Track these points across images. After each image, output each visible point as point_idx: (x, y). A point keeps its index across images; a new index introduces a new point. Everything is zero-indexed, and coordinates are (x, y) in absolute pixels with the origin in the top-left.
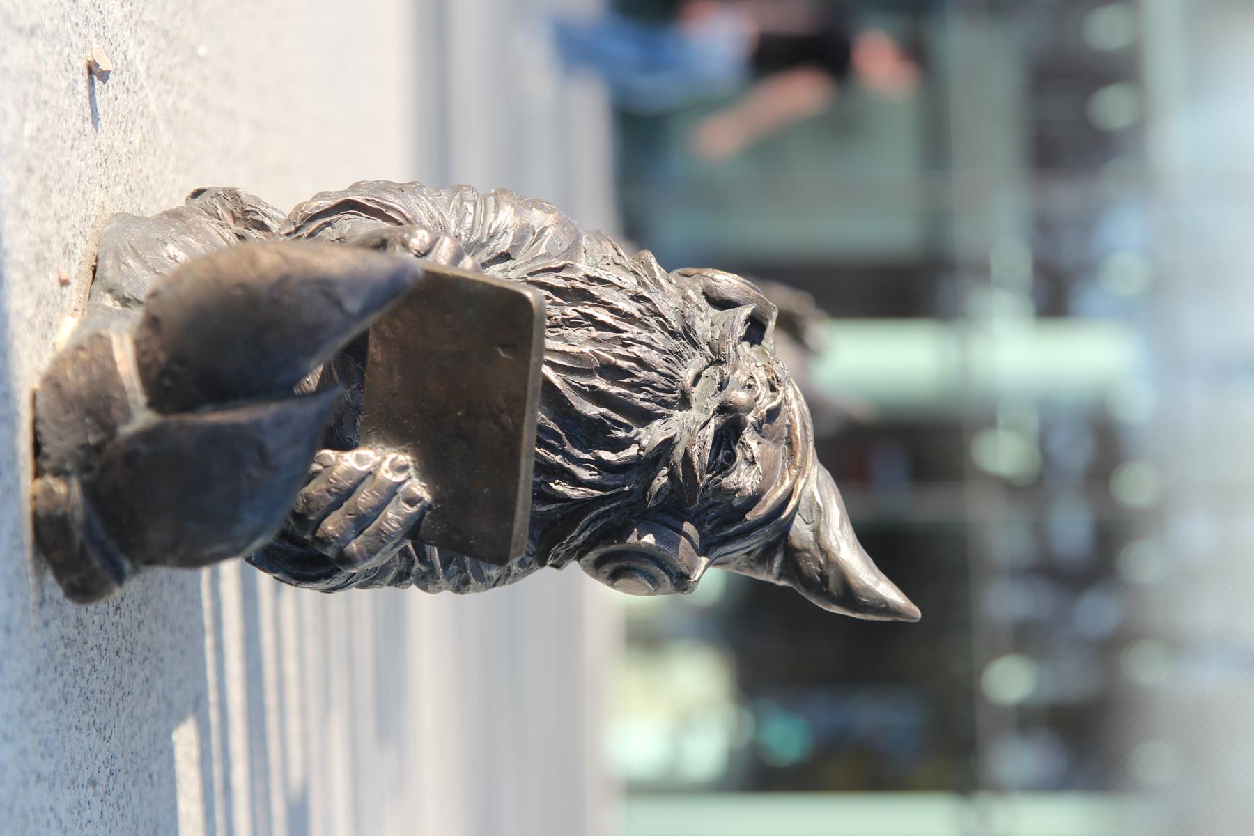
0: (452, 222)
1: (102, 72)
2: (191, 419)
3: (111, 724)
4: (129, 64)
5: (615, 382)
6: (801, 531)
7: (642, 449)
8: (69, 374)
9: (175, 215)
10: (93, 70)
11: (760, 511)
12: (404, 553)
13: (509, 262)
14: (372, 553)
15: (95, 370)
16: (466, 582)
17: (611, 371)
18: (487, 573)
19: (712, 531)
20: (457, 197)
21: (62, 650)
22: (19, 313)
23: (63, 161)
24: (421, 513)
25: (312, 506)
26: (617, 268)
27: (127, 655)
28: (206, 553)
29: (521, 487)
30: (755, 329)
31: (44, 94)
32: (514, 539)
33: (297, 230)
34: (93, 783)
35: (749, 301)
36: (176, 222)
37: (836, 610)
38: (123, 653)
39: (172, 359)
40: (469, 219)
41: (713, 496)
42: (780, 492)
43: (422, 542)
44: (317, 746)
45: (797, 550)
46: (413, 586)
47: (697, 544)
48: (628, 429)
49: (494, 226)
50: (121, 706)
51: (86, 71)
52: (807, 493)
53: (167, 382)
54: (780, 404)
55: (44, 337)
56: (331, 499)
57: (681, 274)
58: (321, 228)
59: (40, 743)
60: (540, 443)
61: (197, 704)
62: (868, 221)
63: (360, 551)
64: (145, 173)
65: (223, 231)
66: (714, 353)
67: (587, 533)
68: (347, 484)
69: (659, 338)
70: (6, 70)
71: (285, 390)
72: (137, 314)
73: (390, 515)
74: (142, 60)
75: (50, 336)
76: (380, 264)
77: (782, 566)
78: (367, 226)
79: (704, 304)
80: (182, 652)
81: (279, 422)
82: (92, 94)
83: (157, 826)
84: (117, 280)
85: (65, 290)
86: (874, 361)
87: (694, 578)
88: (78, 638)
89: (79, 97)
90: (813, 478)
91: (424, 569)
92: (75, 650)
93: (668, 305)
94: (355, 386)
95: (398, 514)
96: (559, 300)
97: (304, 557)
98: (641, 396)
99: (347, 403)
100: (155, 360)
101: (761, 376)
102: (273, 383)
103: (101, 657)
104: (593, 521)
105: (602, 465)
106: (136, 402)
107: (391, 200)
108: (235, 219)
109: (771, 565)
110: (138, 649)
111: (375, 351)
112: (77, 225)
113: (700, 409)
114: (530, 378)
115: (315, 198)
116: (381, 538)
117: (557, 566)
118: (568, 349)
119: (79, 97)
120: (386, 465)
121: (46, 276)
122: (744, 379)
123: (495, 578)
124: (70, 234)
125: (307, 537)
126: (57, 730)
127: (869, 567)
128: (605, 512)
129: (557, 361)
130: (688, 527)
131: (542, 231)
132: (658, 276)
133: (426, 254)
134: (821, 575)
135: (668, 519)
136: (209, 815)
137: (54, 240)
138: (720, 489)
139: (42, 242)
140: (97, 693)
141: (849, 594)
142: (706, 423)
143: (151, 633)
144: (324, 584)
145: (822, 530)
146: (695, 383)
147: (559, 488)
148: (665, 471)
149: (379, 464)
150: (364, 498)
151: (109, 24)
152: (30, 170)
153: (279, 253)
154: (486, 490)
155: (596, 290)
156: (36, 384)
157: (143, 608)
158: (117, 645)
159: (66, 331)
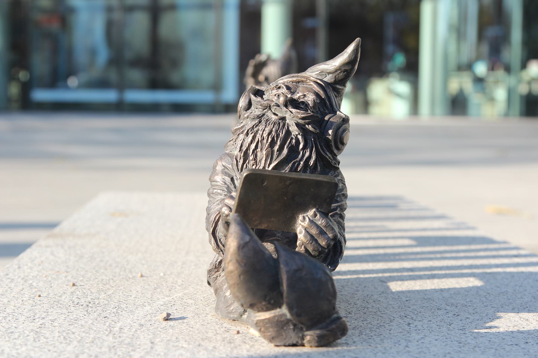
2: (285, 295)
4: (165, 304)
5: (276, 143)
6: (329, 79)
7: (299, 134)
8: (269, 334)
9: (216, 291)
10: (167, 318)
11: (322, 93)
12: (332, 216)
14: (333, 229)
15: (268, 325)
16: (344, 195)
17: (272, 144)
18: (341, 187)
21: (363, 336)
23: (197, 332)
24: (319, 212)
25: (316, 249)
26: (237, 141)
27: (366, 309)
28: (331, 290)
29: (311, 178)
30: (259, 93)
31: (174, 338)
32: (329, 181)
33: (222, 251)
34: (409, 324)
36: (219, 291)
37: (356, 67)
38: (365, 311)
39: (265, 300)
40: (219, 191)
42: (315, 86)
44: (397, 233)
45: (335, 80)
48: (292, 139)
51: (167, 321)
52: (315, 76)
53: (272, 302)
55: (256, 341)
56: (314, 243)
58: (221, 243)
61: (384, 281)
63: (332, 233)
64: (202, 298)
65: (222, 276)
67: (328, 153)
68: (309, 237)
69: (261, 127)
70: (165, 354)
71: (276, 262)
72: (248, 310)
73: (320, 223)
76: (234, 228)
78: (221, 227)
79: (250, 111)
80: (365, 287)
81: (287, 264)
83: (424, 298)
85: (240, 332)
87: (344, 116)
90: (311, 74)
91: (339, 209)
92: (363, 331)
93: (250, 124)
95: (319, 220)
96: (247, 161)
97: (334, 252)
99: (281, 235)
100: (265, 305)
101: (275, 92)
102: (272, 266)
104: (323, 151)
105: (304, 148)
106: (279, 312)
107: (212, 218)
108: (218, 271)
111: (263, 226)
112: (219, 326)
113: (286, 113)
114: (274, 174)
116: (327, 226)
117: (339, 163)
118: (264, 159)
120: (303, 224)
121: (236, 339)
122: (276, 98)
124: (222, 329)
125: (327, 251)
126: (391, 339)
130: (326, 118)
131: (224, 166)
133: (230, 208)
134: (344, 72)
136: (420, 277)
138: (313, 107)
141: (351, 63)
142: (291, 112)
144: (343, 244)
146: (277, 115)
148: (307, 126)
149: (302, 226)
150: (314, 231)
151: (151, 311)
152: (199, 345)
153: (228, 263)
155: (244, 149)
156: (272, 345)
157: (349, 303)
159: (254, 332)
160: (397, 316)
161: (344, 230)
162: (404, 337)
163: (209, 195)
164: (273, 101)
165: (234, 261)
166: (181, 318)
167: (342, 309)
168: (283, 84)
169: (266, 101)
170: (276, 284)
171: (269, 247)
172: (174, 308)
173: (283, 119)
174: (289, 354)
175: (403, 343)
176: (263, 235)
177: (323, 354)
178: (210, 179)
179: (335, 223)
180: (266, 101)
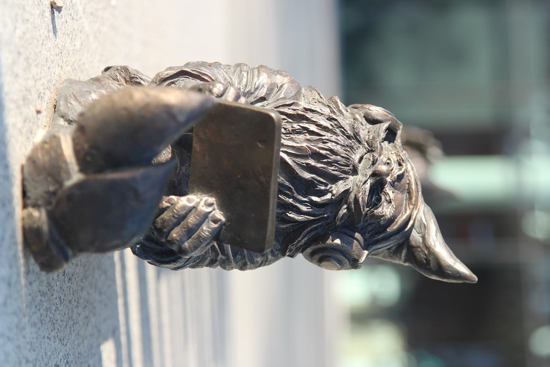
0: (236, 82)
1: (58, 7)
3: (67, 338)
5: (319, 162)
6: (416, 237)
9: (97, 80)
10: (54, 8)
11: (394, 227)
13: (265, 102)
14: (196, 248)
15: (53, 153)
17: (317, 156)
18: (256, 259)
19: (370, 237)
20: (239, 69)
21: (39, 297)
22: (14, 125)
23: (37, 51)
25: (165, 224)
27: (75, 304)
30: (391, 135)
31: (27, 16)
32: (267, 239)
35: (388, 120)
38: (73, 302)
40: (244, 80)
41: (370, 219)
43: (221, 242)
45: (413, 247)
46: (219, 267)
47: (362, 244)
48: (326, 185)
49: (257, 84)
50: (72, 329)
52: (418, 218)
53: (89, 158)
54: (404, 172)
55: (28, 138)
57: (352, 107)
59: (28, 343)
60: (280, 192)
61: (114, 333)
62: (472, 111)
63: (189, 247)
66: (369, 146)
67: (306, 239)
69: (341, 139)
72: (74, 126)
73: (205, 228)
74: (81, 4)
75: (31, 138)
77: (406, 255)
79: (364, 122)
82: (53, 19)
84: (66, 111)
85: (39, 116)
86: (471, 179)
88: (48, 292)
89: (46, 19)
90: (422, 210)
91: (224, 258)
93: (346, 122)
94: (187, 165)
95: (209, 228)
96: (290, 120)
97: (162, 251)
98: (332, 168)
101: (394, 158)
103: (61, 303)
105: (313, 204)
107: (204, 70)
108: (126, 81)
109: (401, 255)
110: (81, 301)
111: (196, 146)
112: (46, 84)
113: (363, 175)
115: (167, 70)
117: (292, 256)
119: (46, 19)
120: (202, 203)
121: (29, 108)
122: (385, 160)
123: (260, 262)
124: (41, 88)
125: (163, 240)
126: (37, 338)
127: (451, 255)
128: (315, 228)
129: (290, 151)
130: (357, 235)
131: (282, 86)
132: (341, 108)
133: (221, 96)
134: (426, 260)
135: (347, 231)
137: (33, 91)
139: (26, 90)
140: (59, 322)
141: (440, 269)
142: (366, 182)
143: (88, 293)
144: (172, 266)
145: (426, 236)
147: (292, 216)
148: (345, 206)
149: (199, 203)
150: (191, 220)
152: (19, 53)
154: (253, 215)
155: (309, 115)
156: (23, 161)
157: (84, 280)
158: (70, 298)
159: (40, 135)
160: (68, 350)
161: (193, 267)
162: (40, 358)
163: (238, 65)
164: (380, 155)
165: (147, 100)
166: (54, 27)
167: (78, 264)
168: (406, 170)
169: (380, 145)
170: (115, 163)
171: (166, 154)
172: (68, 18)
173: (355, 171)
174: (11, 186)
175: (32, 356)
176: (183, 146)
177: (13, 236)
178: (262, 66)
179: (203, 253)
180: (380, 145)
